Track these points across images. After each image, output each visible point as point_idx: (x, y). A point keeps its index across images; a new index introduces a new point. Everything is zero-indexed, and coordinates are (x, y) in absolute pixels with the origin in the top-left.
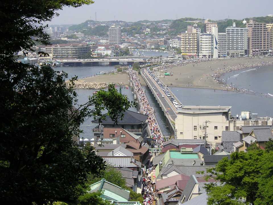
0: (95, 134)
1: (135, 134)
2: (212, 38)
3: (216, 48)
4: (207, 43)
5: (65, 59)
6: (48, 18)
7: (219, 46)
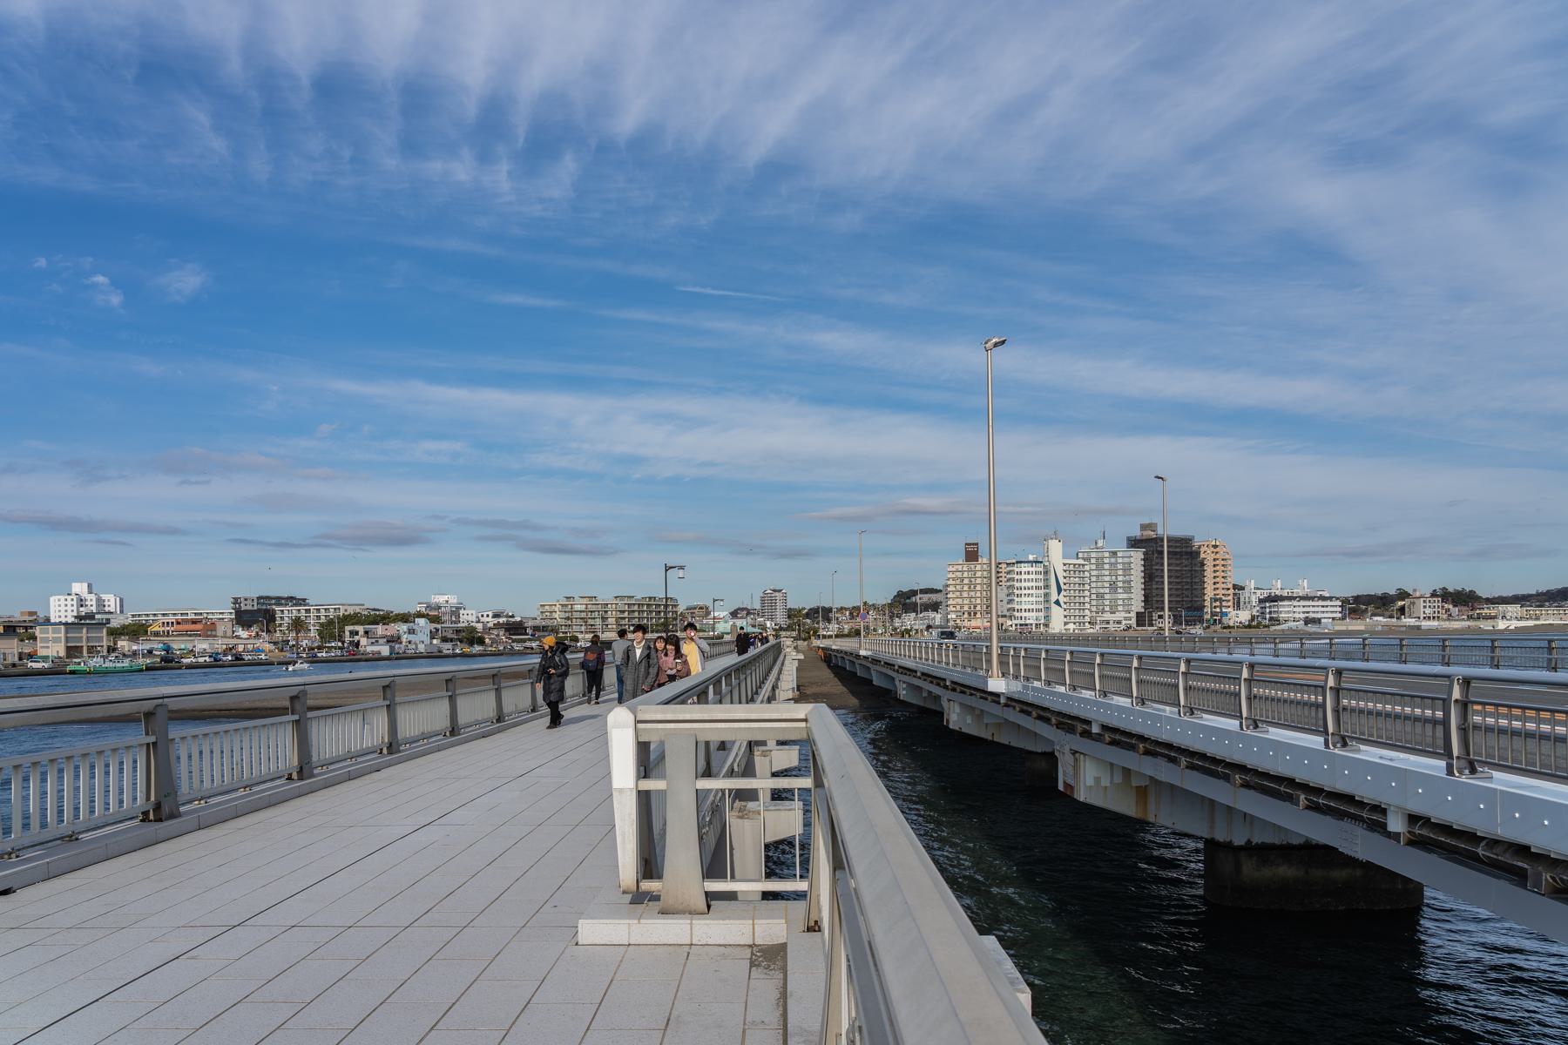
0: (766, 745)
1: (668, 702)
2: (1046, 573)
3: (1057, 603)
4: (1025, 589)
5: (1456, 630)
6: (786, 871)
7: (1065, 596)
